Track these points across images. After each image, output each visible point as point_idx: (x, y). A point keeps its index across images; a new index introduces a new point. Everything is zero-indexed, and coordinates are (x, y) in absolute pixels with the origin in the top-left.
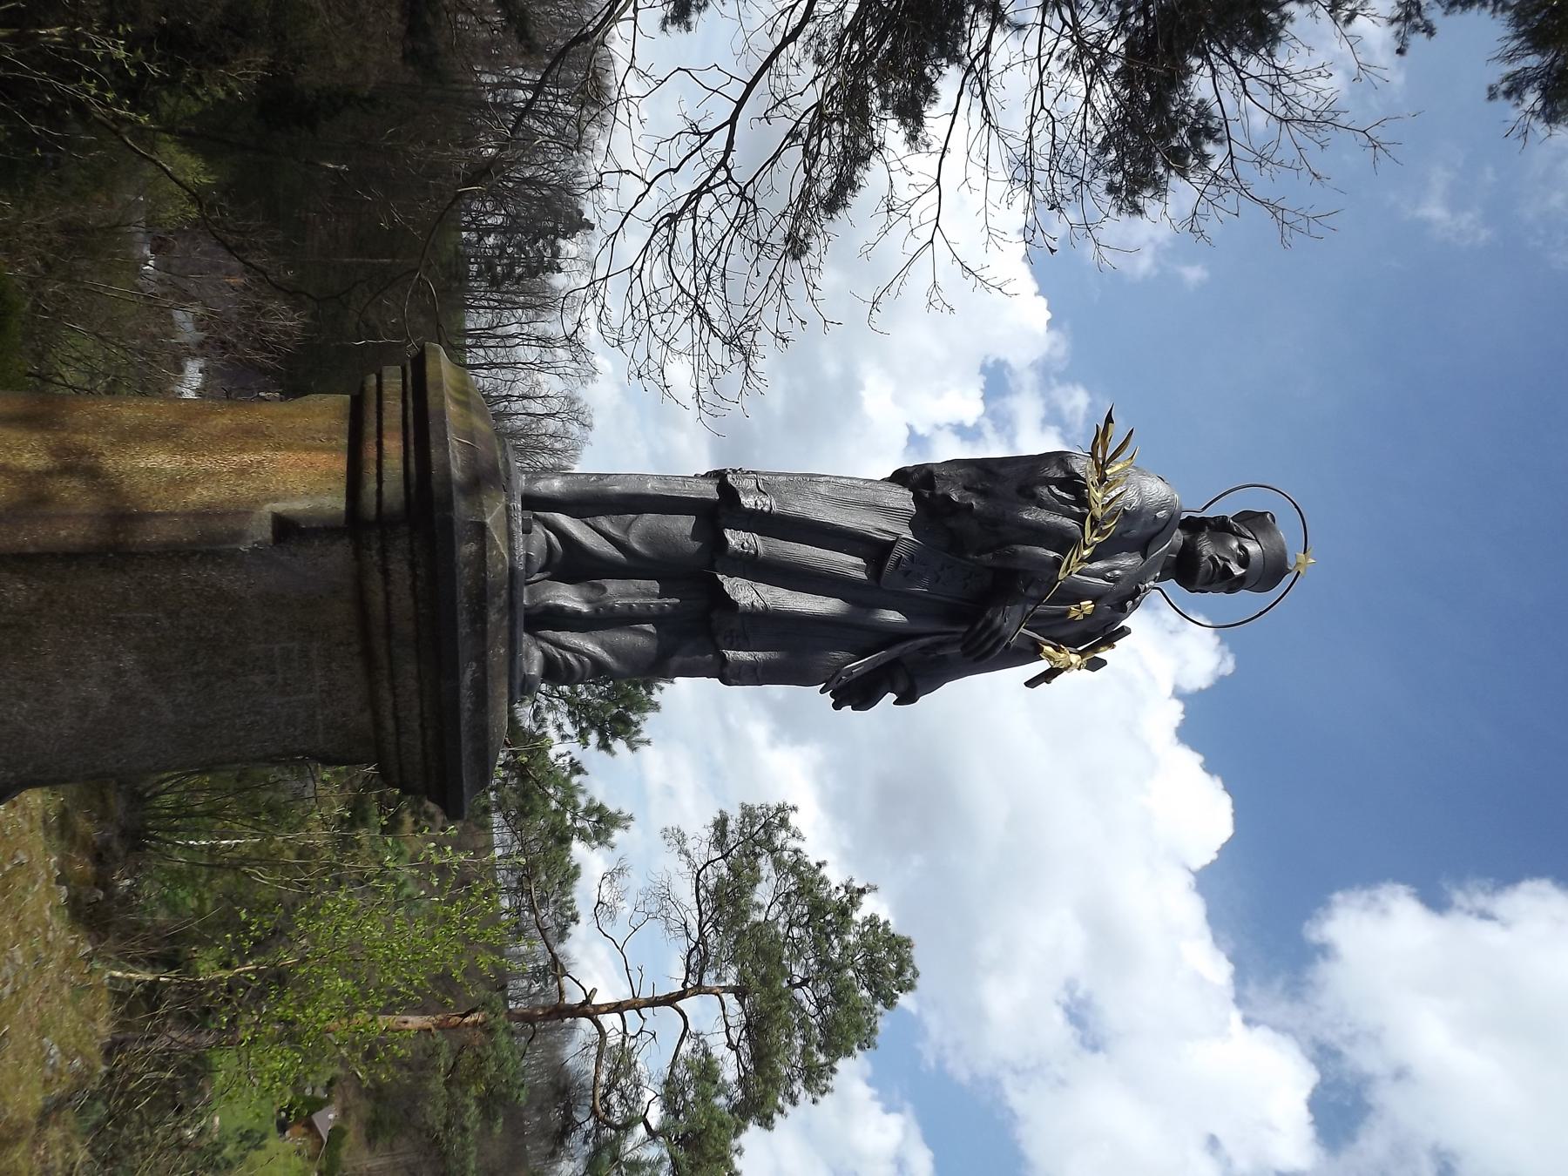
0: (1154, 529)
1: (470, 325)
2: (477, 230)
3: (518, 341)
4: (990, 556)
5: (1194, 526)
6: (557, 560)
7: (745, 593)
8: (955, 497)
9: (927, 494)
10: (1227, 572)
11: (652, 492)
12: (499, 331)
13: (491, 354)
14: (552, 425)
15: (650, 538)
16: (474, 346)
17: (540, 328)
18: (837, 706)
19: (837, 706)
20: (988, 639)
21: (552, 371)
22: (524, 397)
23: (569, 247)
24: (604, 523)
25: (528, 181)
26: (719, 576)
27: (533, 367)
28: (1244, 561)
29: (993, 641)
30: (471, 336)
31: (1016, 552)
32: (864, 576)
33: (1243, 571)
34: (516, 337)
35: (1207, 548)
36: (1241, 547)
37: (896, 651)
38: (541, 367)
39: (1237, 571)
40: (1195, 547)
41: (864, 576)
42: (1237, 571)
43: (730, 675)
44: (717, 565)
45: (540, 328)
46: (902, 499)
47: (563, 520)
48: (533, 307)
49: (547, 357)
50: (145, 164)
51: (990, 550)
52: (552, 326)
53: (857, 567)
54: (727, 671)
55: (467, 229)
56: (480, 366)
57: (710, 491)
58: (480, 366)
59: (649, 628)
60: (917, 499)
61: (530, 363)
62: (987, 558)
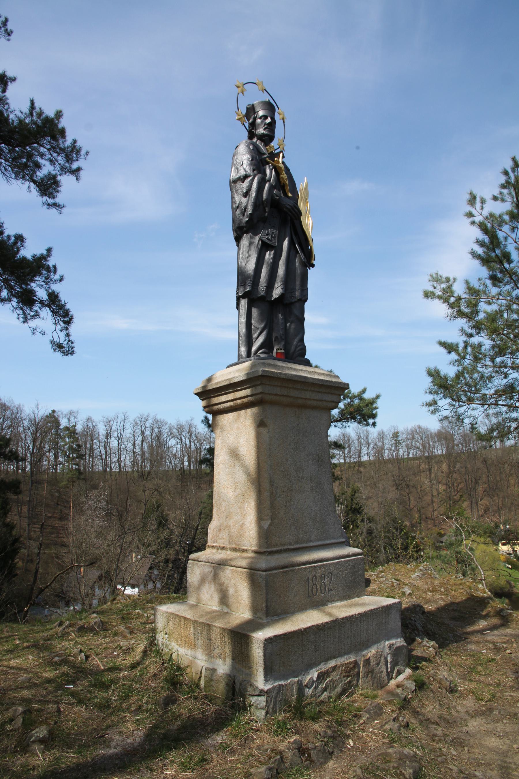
0: (255, 149)
1: (101, 469)
2: (57, 466)
3: (108, 448)
4: (266, 208)
5: (251, 135)
6: (267, 351)
7: (277, 292)
8: (247, 219)
9: (245, 229)
10: (269, 124)
11: (245, 320)
12: (104, 456)
13: (114, 460)
14: (147, 433)
15: (261, 320)
16: (111, 467)
17: (102, 437)
18: (313, 266)
19: (313, 266)
20: (294, 211)
21: (122, 432)
22: (134, 445)
23: (64, 423)
24: (255, 336)
25: (34, 441)
26: (273, 299)
27: (120, 441)
28: (265, 117)
29: (295, 209)
30: (106, 469)
31: (266, 199)
32: (273, 252)
33: (269, 118)
34: (106, 448)
35: (261, 131)
36: (260, 118)
37: (296, 242)
38: (120, 438)
39: (269, 120)
40: (260, 135)
41: (273, 252)
42: (269, 120)
43: (304, 299)
44: (269, 300)
45: (102, 437)
46: (245, 241)
47: (254, 349)
48: (92, 440)
49: (115, 434)
50: (130, 490)
51: (264, 208)
52: (102, 430)
53: (270, 254)
54: (303, 299)
55: (56, 469)
56: (120, 465)
57: (244, 303)
58: (120, 465)
59: (288, 324)
60: (247, 232)
61: (118, 442)
62: (267, 209)
